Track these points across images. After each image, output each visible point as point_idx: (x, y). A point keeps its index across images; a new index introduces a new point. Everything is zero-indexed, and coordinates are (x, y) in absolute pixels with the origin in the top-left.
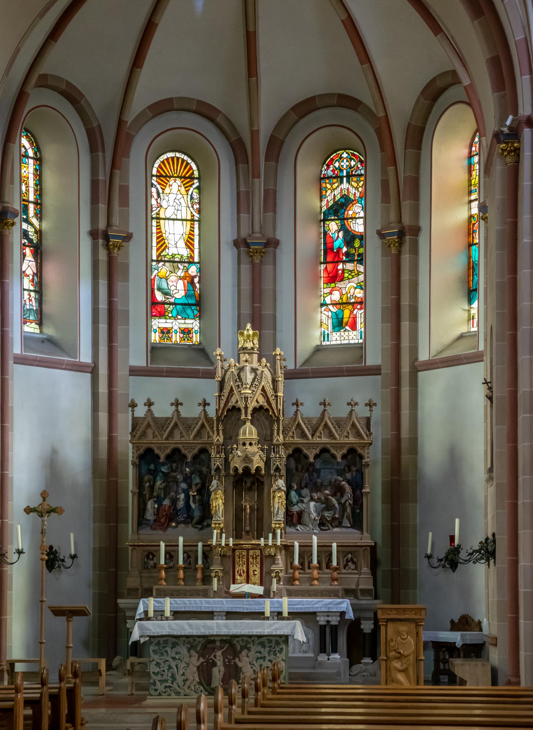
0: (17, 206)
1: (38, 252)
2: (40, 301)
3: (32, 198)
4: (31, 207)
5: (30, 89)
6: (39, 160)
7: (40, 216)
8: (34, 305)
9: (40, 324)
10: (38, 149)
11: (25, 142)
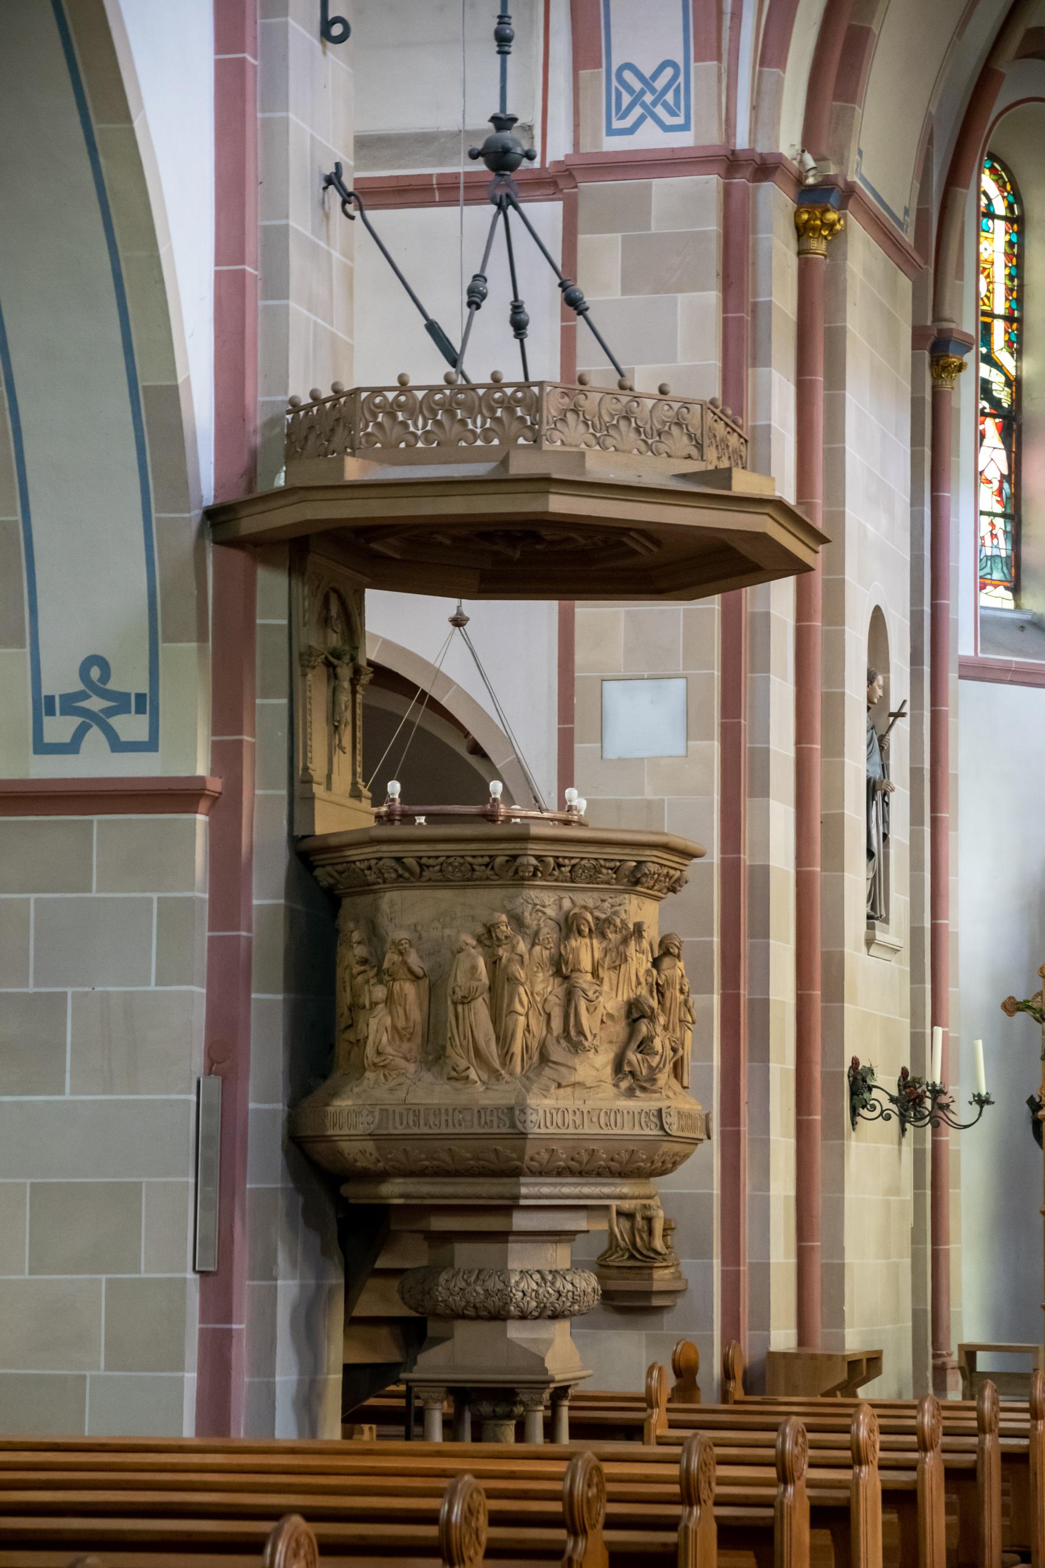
0: (969, 327)
1: (1013, 426)
2: (1016, 538)
3: (1000, 306)
4: (999, 328)
5: (1005, 64)
6: (1017, 221)
7: (1017, 347)
8: (1003, 547)
9: (1016, 588)
10: (1016, 197)
11: (988, 183)
